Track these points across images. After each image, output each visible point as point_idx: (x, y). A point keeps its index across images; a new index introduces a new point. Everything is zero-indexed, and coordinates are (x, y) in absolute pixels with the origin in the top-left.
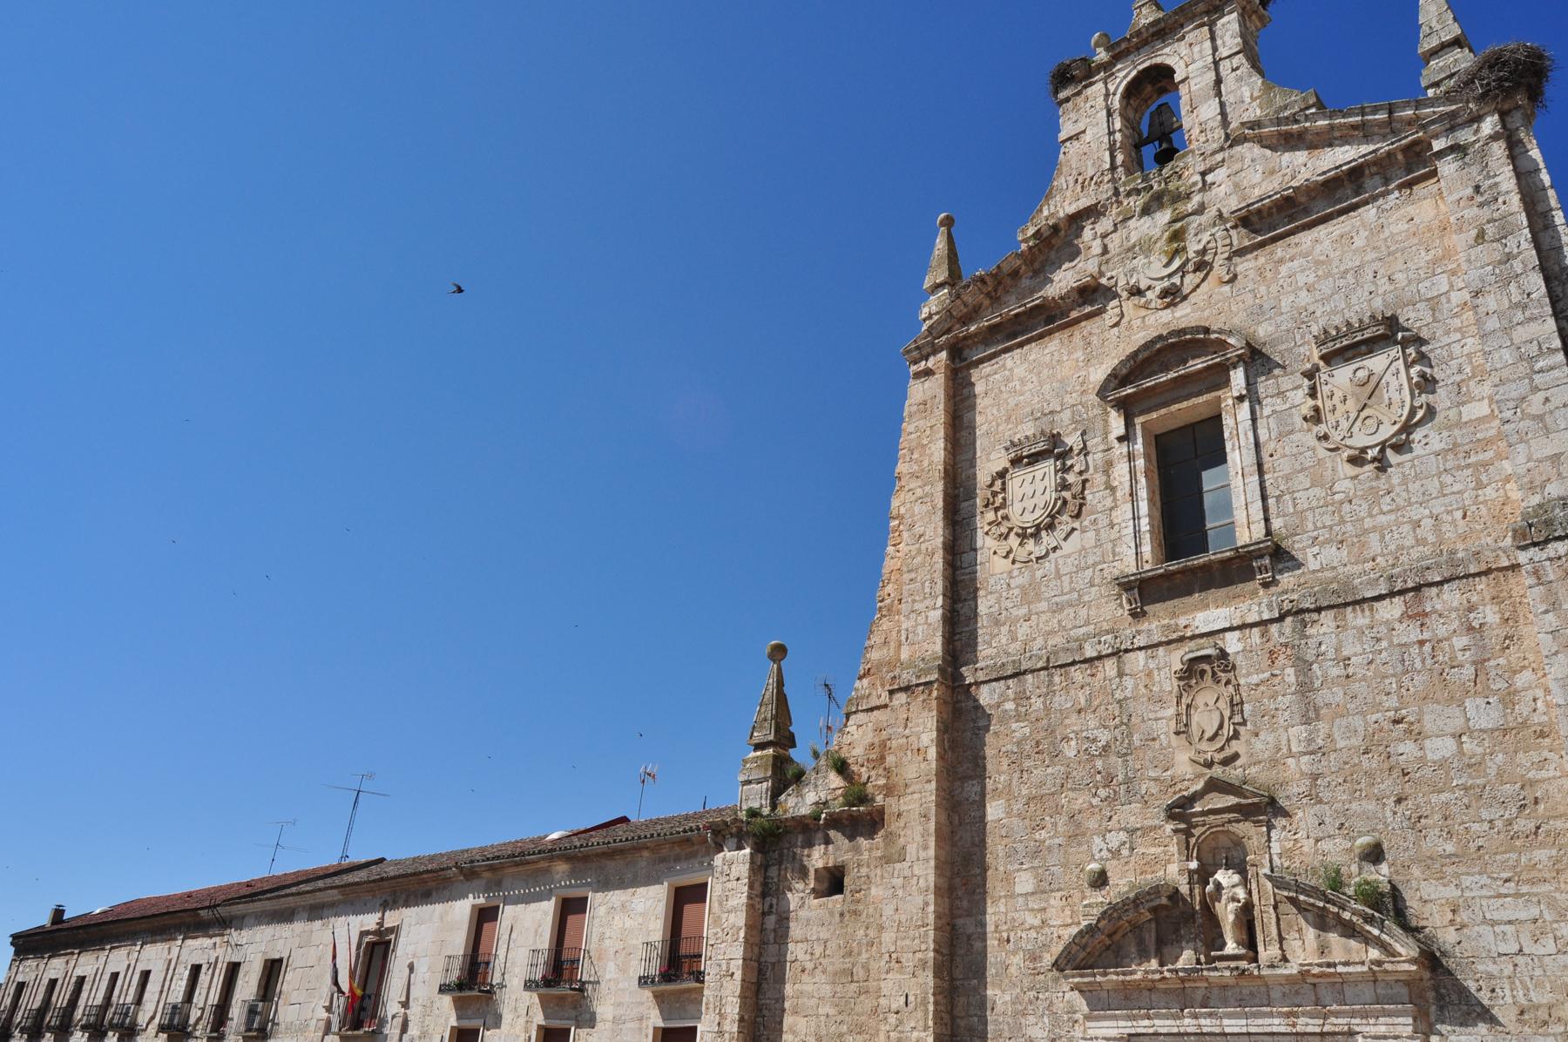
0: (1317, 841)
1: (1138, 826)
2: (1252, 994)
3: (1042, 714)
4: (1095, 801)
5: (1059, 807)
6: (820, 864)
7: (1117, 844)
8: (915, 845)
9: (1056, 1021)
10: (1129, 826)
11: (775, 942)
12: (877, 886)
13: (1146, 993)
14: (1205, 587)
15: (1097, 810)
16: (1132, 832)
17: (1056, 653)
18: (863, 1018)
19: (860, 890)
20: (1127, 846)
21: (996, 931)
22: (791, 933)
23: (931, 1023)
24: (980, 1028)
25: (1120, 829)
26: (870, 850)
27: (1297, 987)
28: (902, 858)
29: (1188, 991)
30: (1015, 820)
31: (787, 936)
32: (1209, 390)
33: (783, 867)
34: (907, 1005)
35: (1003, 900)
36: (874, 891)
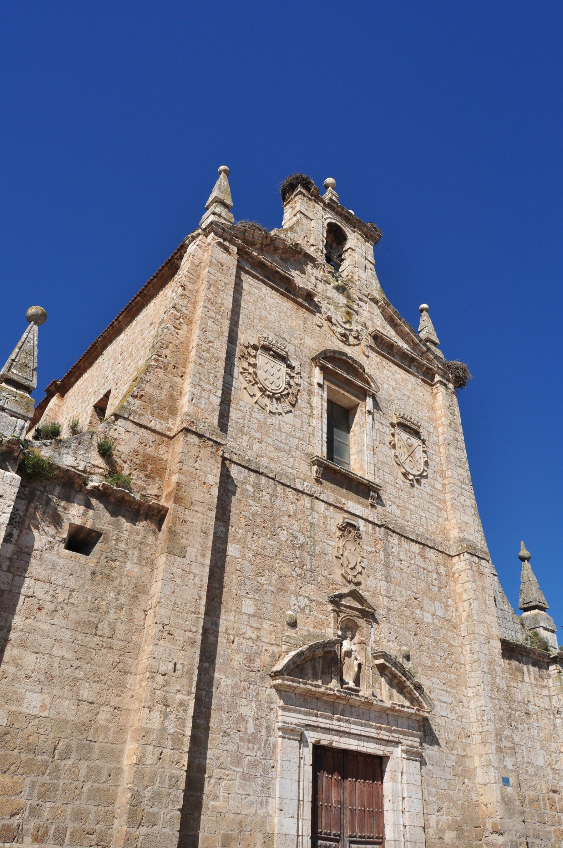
0: (388, 641)
1: (315, 599)
2: (363, 713)
3: (268, 505)
4: (294, 574)
5: (274, 568)
6: (77, 521)
7: (304, 605)
8: (195, 550)
9: (259, 708)
10: (310, 597)
11: (9, 571)
12: (133, 563)
13: (315, 700)
14: (349, 489)
15: (294, 580)
16: (311, 601)
17: (281, 474)
18: (103, 669)
19: (115, 560)
20: (309, 608)
21: (226, 633)
22: (30, 569)
23: (194, 690)
24: (207, 700)
25: (306, 597)
26: (131, 532)
27: (381, 714)
28: (182, 554)
29: (336, 704)
30: (247, 564)
31: (26, 570)
32: (357, 397)
33: (33, 505)
34: (174, 671)
35: (233, 613)
36: (129, 565)
